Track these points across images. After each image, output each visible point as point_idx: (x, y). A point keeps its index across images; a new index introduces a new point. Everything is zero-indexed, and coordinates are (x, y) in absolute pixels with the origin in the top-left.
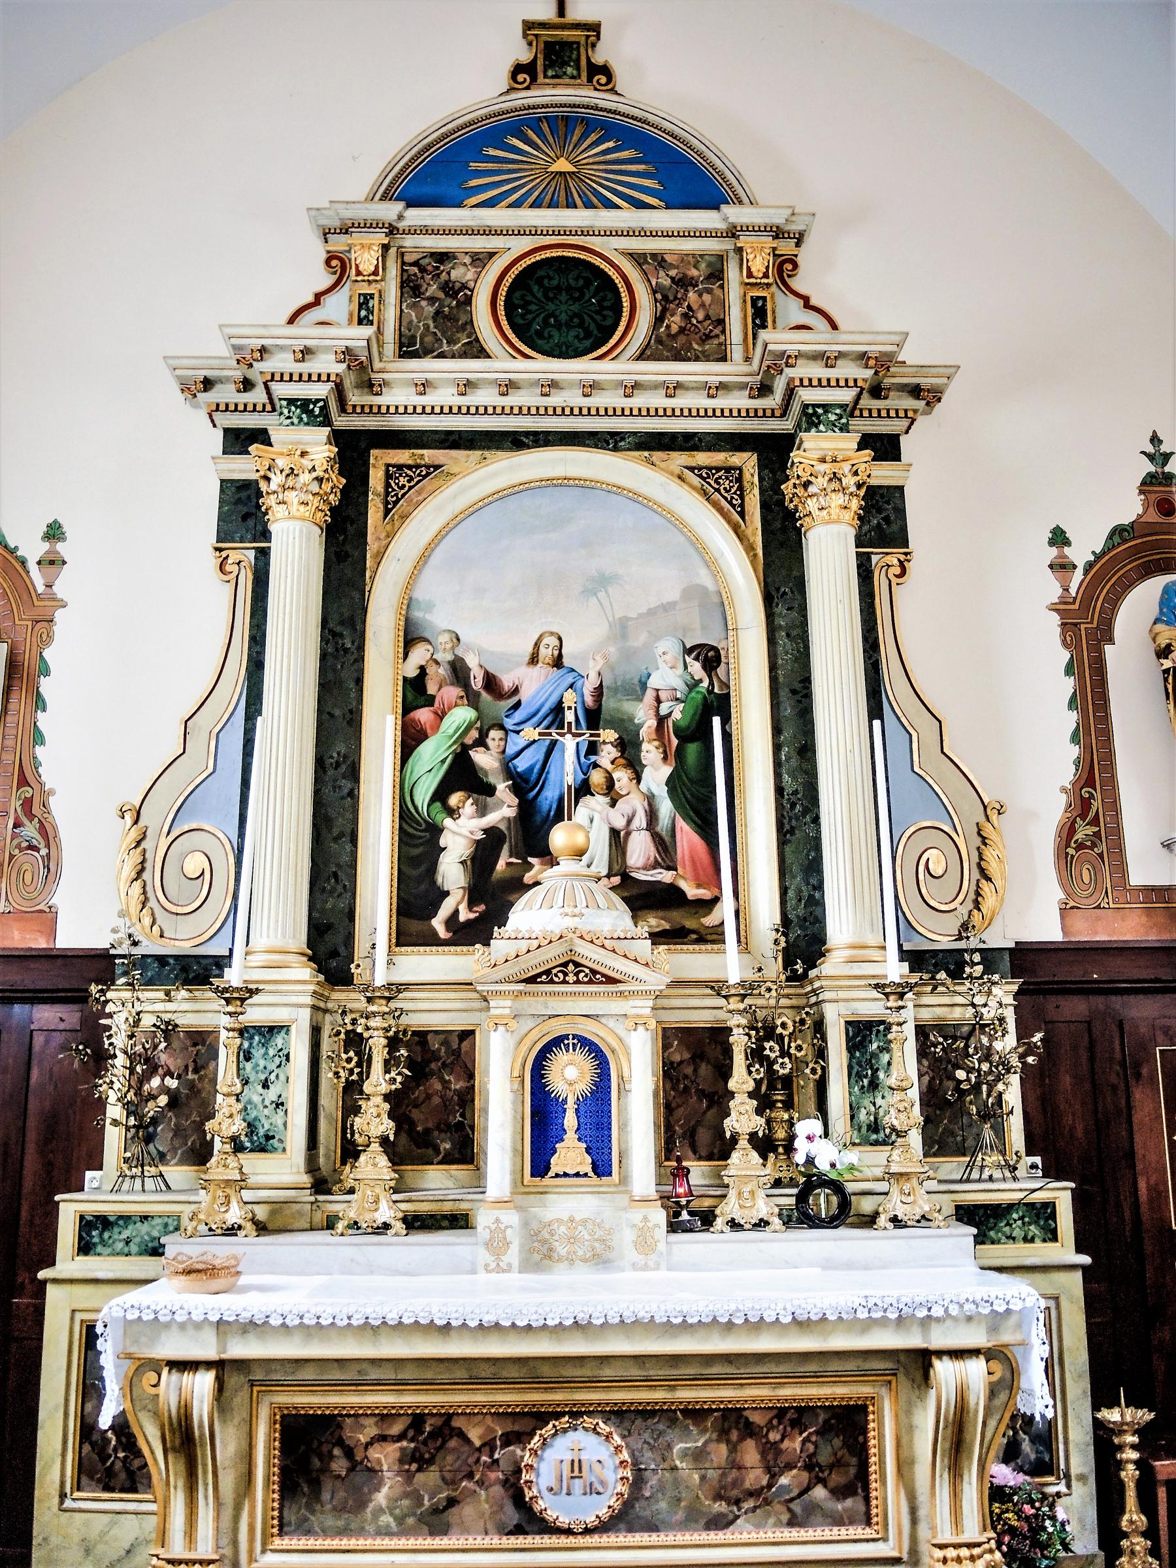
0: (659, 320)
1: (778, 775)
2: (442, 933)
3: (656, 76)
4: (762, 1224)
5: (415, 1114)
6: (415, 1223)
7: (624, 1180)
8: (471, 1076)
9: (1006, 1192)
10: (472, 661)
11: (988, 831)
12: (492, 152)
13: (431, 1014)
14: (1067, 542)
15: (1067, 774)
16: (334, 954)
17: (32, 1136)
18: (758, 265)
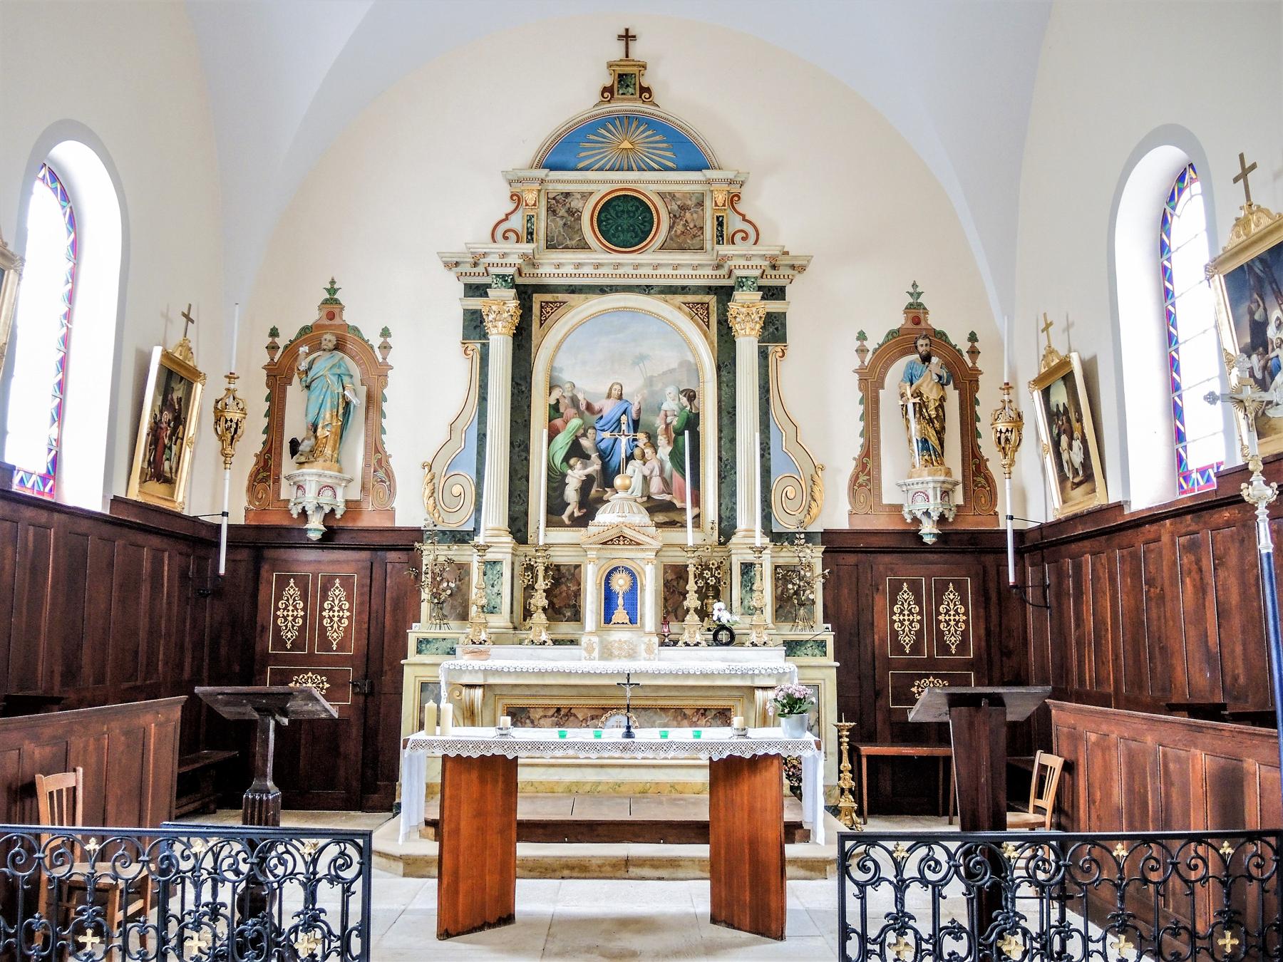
0: (671, 228)
1: (719, 451)
2: (567, 522)
3: (679, 93)
4: (697, 644)
5: (555, 600)
6: (555, 642)
7: (643, 626)
8: (579, 584)
9: (806, 635)
10: (580, 397)
11: (816, 478)
12: (592, 137)
13: (562, 557)
14: (865, 339)
15: (857, 452)
16: (519, 530)
17: (388, 608)
18: (720, 198)
